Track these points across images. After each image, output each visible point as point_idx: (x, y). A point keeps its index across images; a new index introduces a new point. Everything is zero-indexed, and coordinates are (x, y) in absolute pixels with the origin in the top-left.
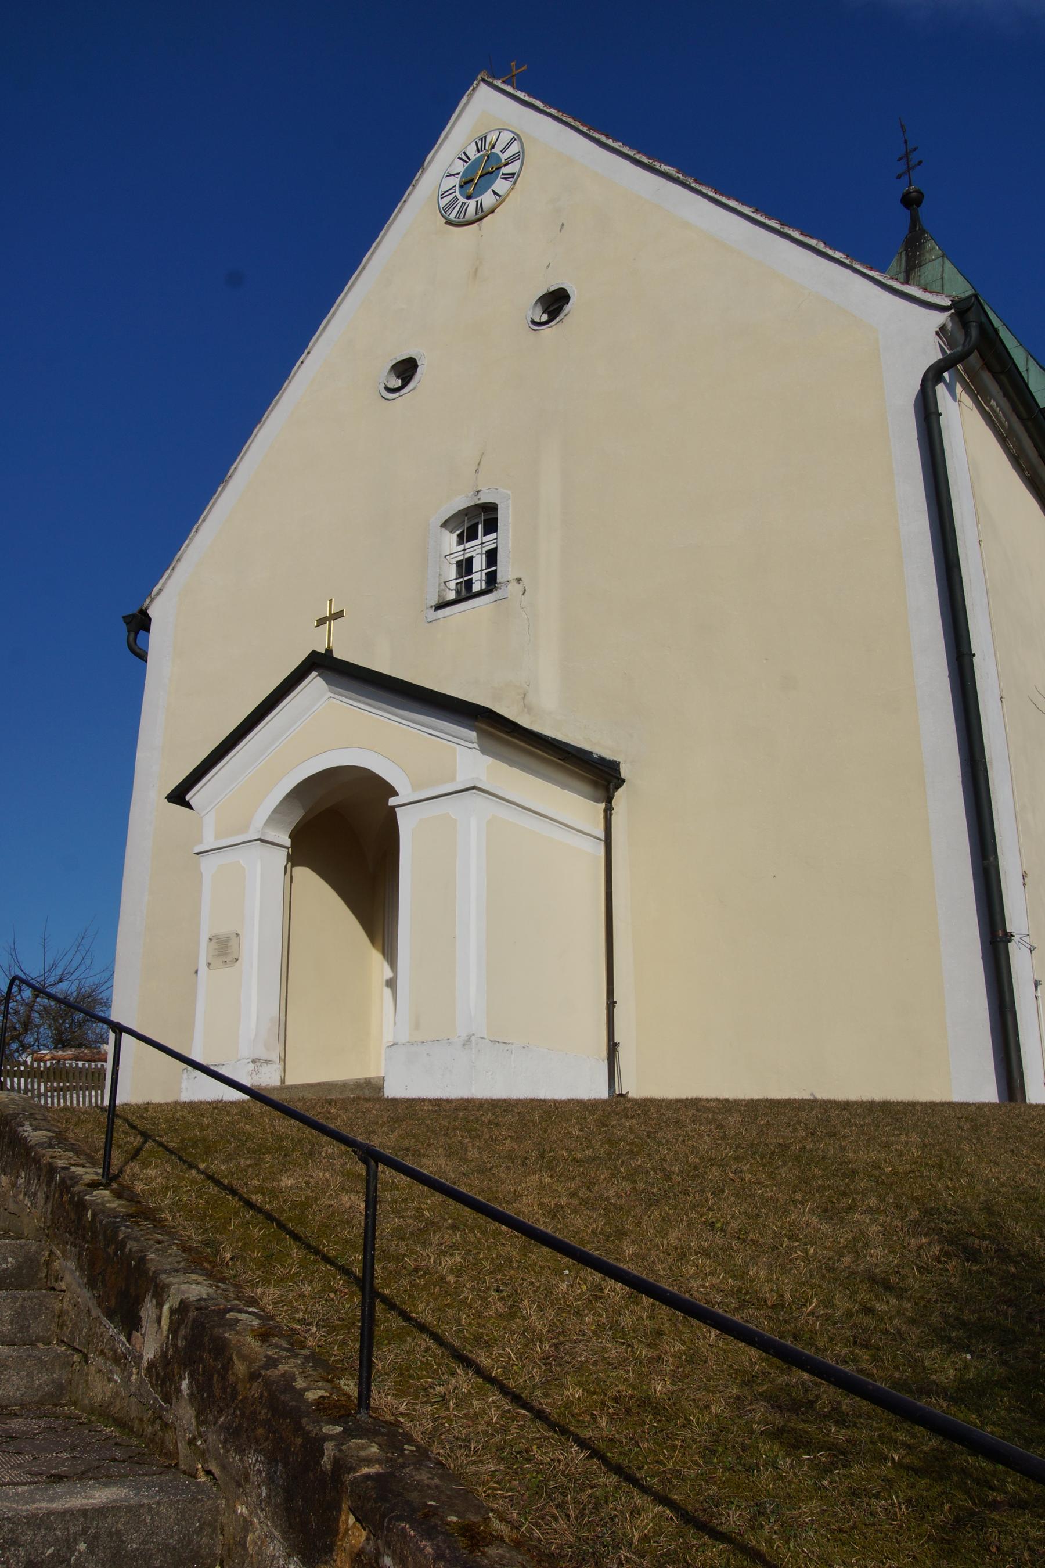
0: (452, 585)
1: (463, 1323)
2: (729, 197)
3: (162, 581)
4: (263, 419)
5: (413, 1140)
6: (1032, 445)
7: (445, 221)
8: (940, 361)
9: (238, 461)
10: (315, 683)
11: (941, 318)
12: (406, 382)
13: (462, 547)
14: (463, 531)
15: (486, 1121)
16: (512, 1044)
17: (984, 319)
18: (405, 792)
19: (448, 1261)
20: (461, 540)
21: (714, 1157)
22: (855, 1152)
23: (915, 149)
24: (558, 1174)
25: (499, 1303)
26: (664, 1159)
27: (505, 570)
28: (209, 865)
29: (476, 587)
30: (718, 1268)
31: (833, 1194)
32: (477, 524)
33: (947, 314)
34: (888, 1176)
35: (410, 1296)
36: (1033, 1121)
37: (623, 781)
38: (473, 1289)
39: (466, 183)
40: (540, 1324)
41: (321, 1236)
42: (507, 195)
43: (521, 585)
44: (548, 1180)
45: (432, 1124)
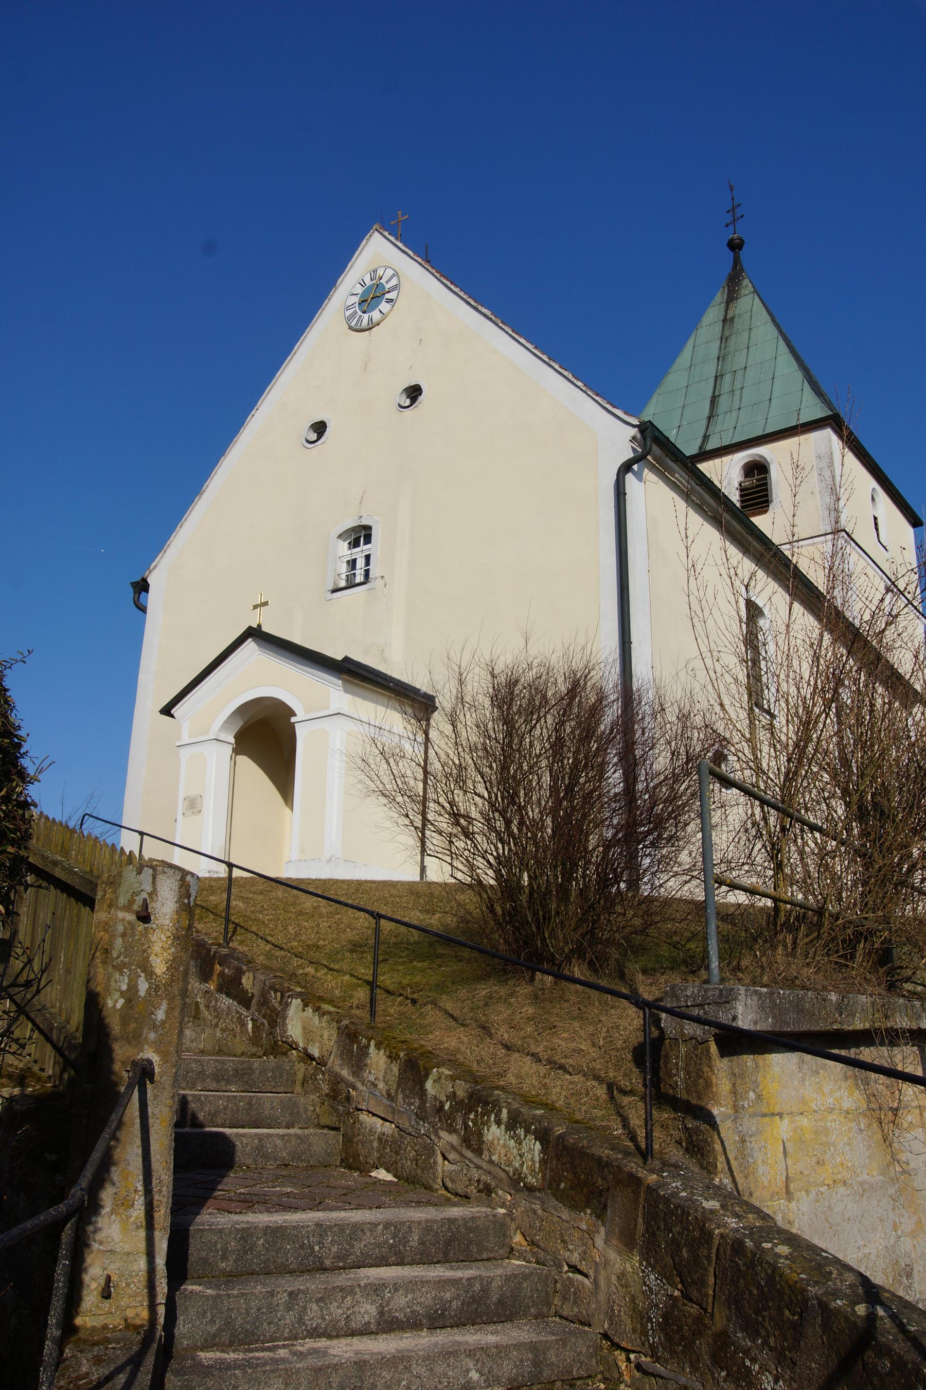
0: (344, 576)
2: (520, 336)
3: (157, 560)
13: (350, 552)
18: (300, 714)
23: (739, 205)
28: (185, 753)
42: (388, 314)
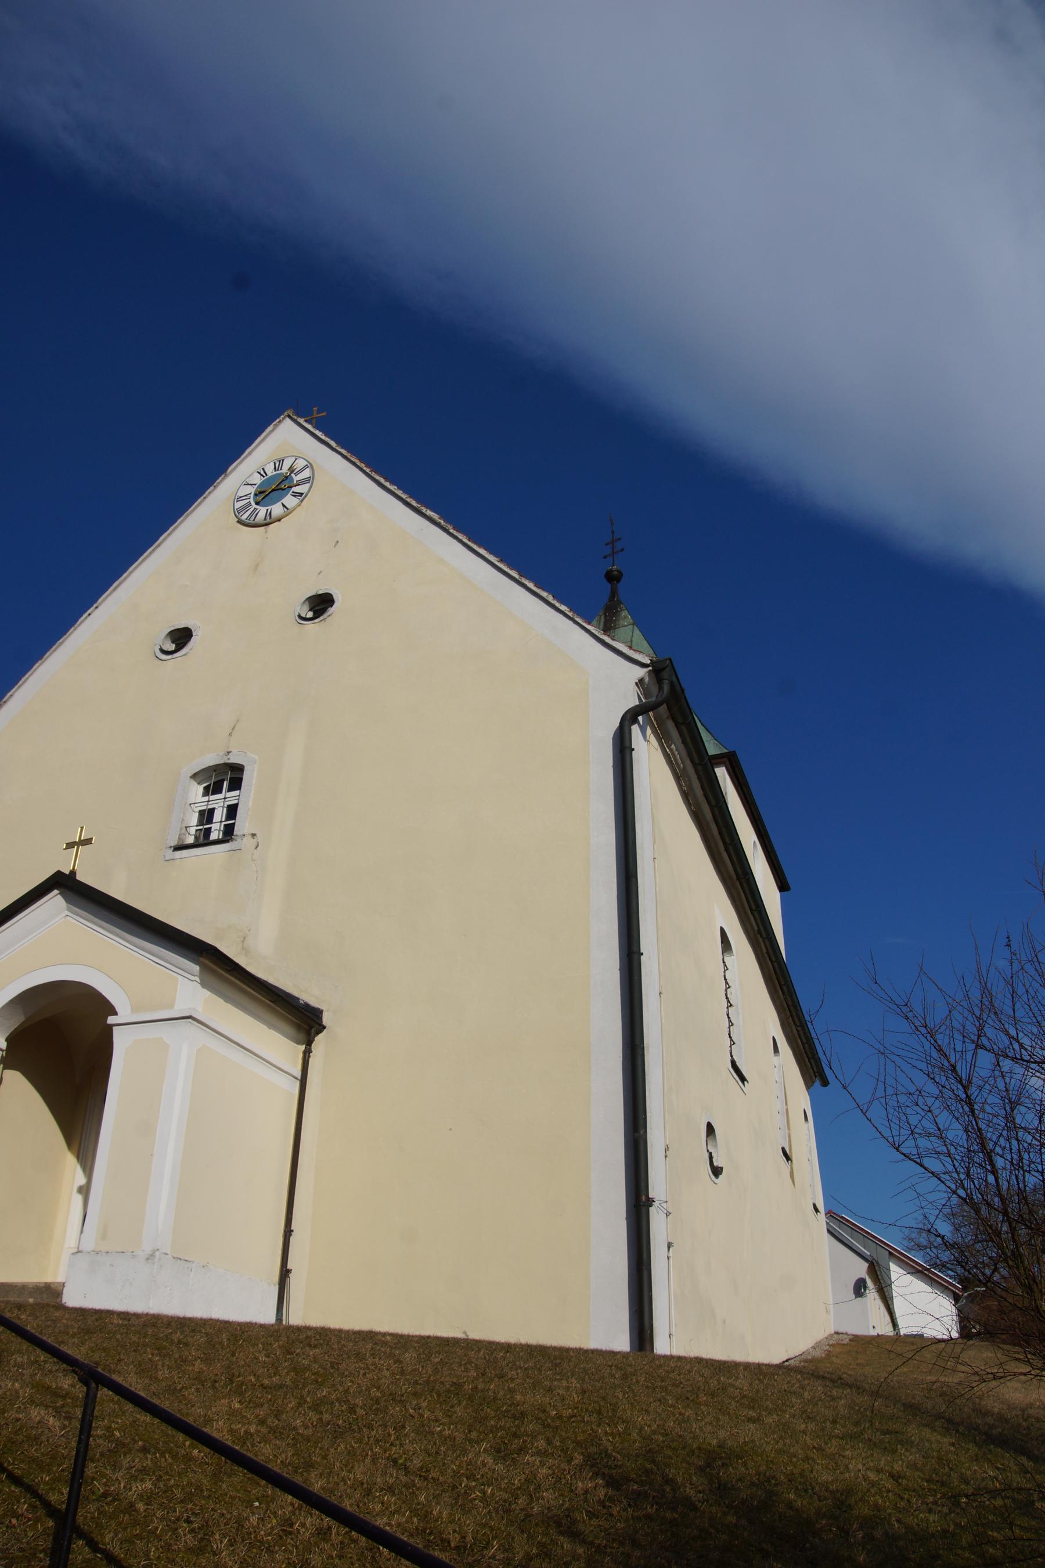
0: (193, 830)
1: (152, 1557)
2: (480, 546)
4: (45, 657)
5: (104, 1354)
6: (699, 785)
7: (237, 520)
8: (636, 706)
9: (14, 689)
10: (55, 900)
11: (641, 672)
12: (180, 646)
13: (206, 799)
14: (210, 785)
15: (176, 1340)
16: (193, 1262)
17: (674, 679)
18: (124, 1012)
19: (138, 1487)
20: (207, 792)
21: (394, 1392)
22: (522, 1395)
23: (619, 539)
24: (247, 1400)
25: (189, 1536)
26: (347, 1391)
27: (242, 824)
29: (214, 836)
30: (403, 1506)
31: (505, 1435)
32: (223, 781)
33: (646, 670)
34: (553, 1419)
35: (97, 1524)
36: (673, 1372)
37: (324, 1027)
38: (162, 1519)
39: (261, 493)
40: (230, 1560)
41: (6, 1453)
42: (294, 509)
43: (255, 840)
44: (237, 1405)
45: (122, 1339)
